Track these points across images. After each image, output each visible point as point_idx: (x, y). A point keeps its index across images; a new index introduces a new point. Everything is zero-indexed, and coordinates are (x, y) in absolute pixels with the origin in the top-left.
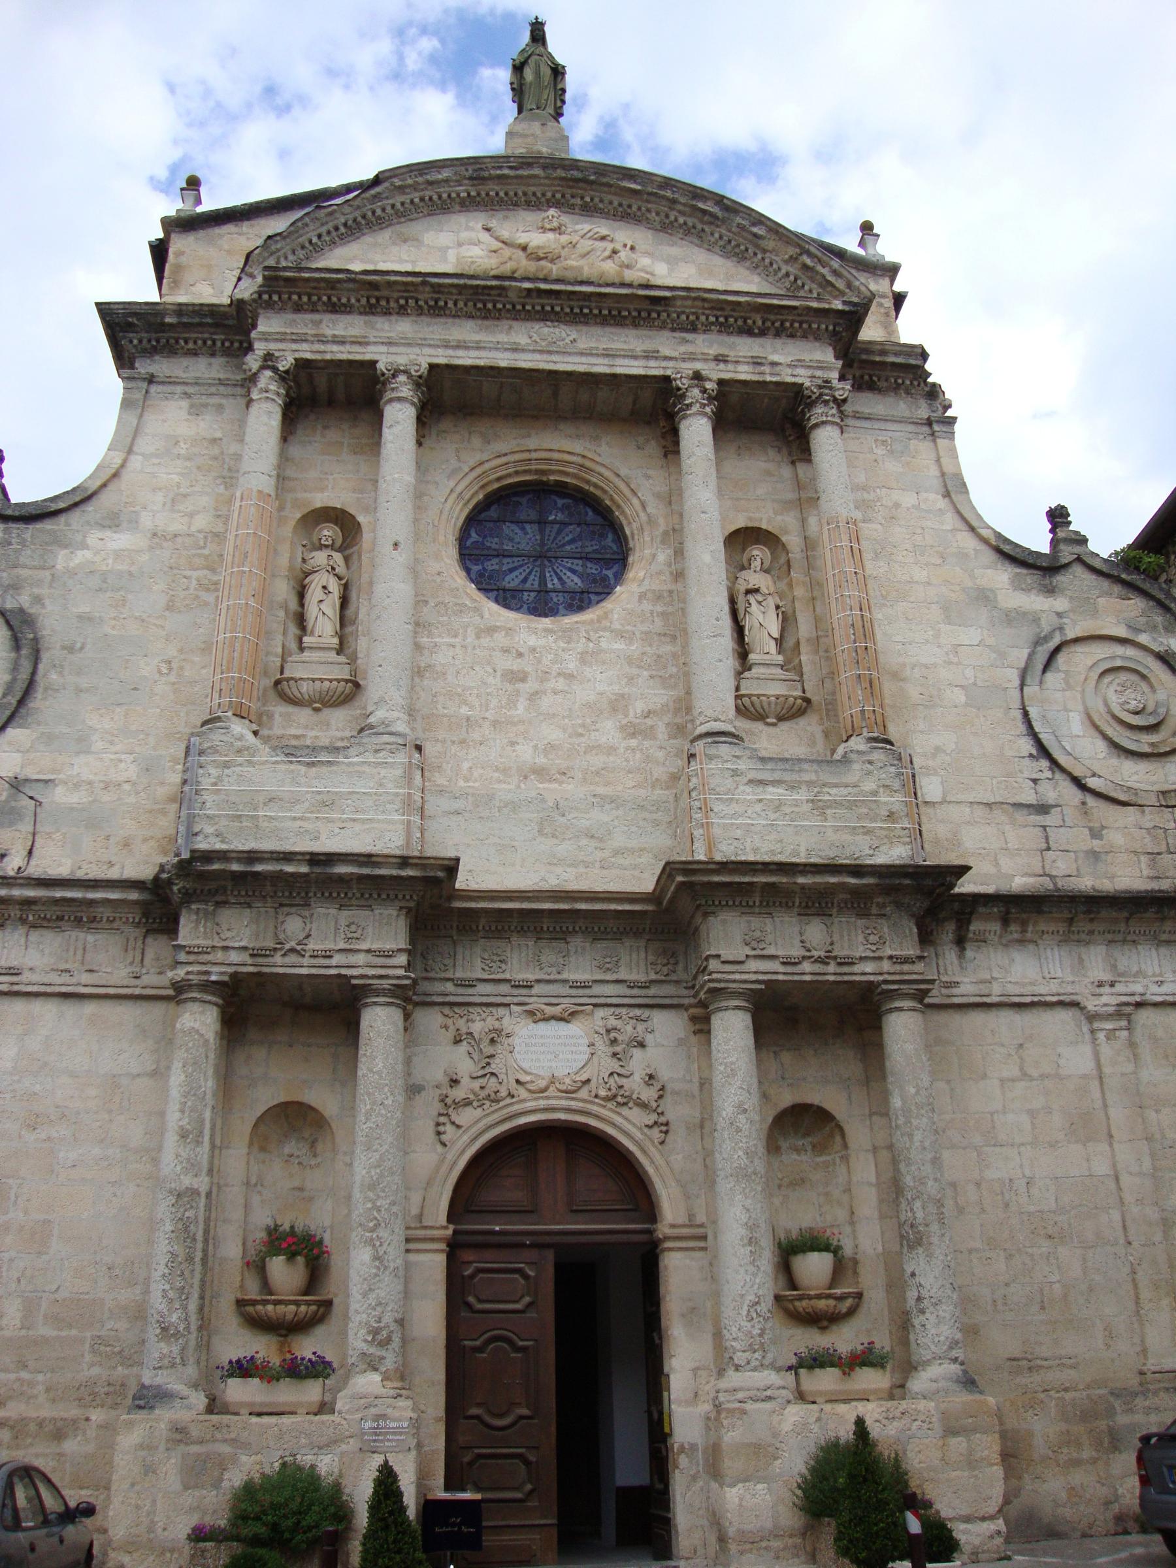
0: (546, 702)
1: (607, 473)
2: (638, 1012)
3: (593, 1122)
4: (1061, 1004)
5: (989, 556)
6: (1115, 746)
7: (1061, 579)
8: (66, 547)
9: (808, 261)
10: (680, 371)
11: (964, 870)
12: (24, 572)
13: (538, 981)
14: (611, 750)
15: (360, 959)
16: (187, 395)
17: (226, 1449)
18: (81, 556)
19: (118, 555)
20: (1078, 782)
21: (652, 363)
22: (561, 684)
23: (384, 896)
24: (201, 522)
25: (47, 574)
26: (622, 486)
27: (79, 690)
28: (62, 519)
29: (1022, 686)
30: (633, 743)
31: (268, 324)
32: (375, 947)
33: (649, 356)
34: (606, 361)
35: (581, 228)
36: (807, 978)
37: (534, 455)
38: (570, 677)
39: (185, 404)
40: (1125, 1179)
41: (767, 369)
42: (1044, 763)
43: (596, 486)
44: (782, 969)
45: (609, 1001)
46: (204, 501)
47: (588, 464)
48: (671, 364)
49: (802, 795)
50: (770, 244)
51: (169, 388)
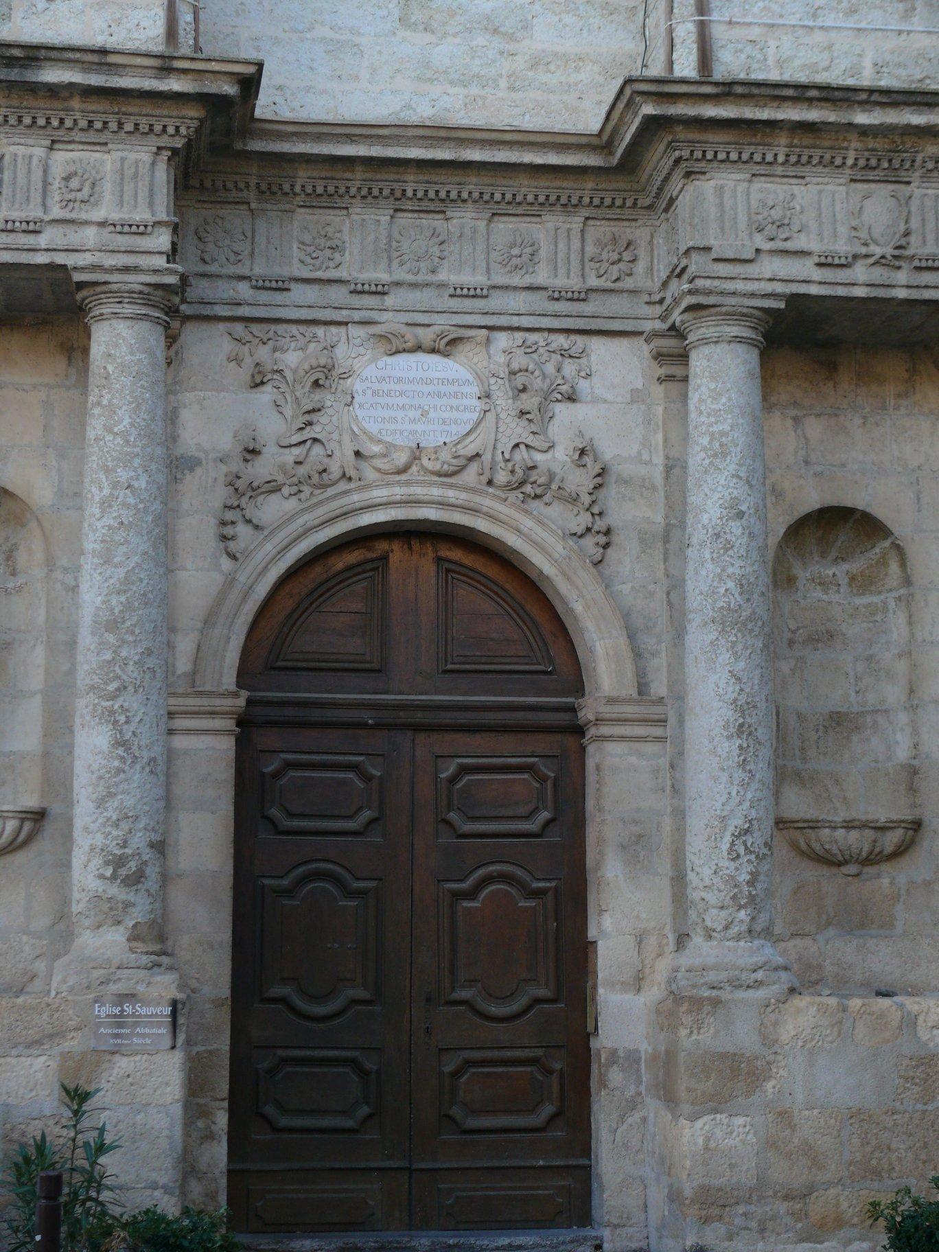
2: (561, 341)
13: (398, 284)
23: (129, 127)
32: (561, 282)
36: (860, 292)
44: (817, 274)
45: (515, 321)
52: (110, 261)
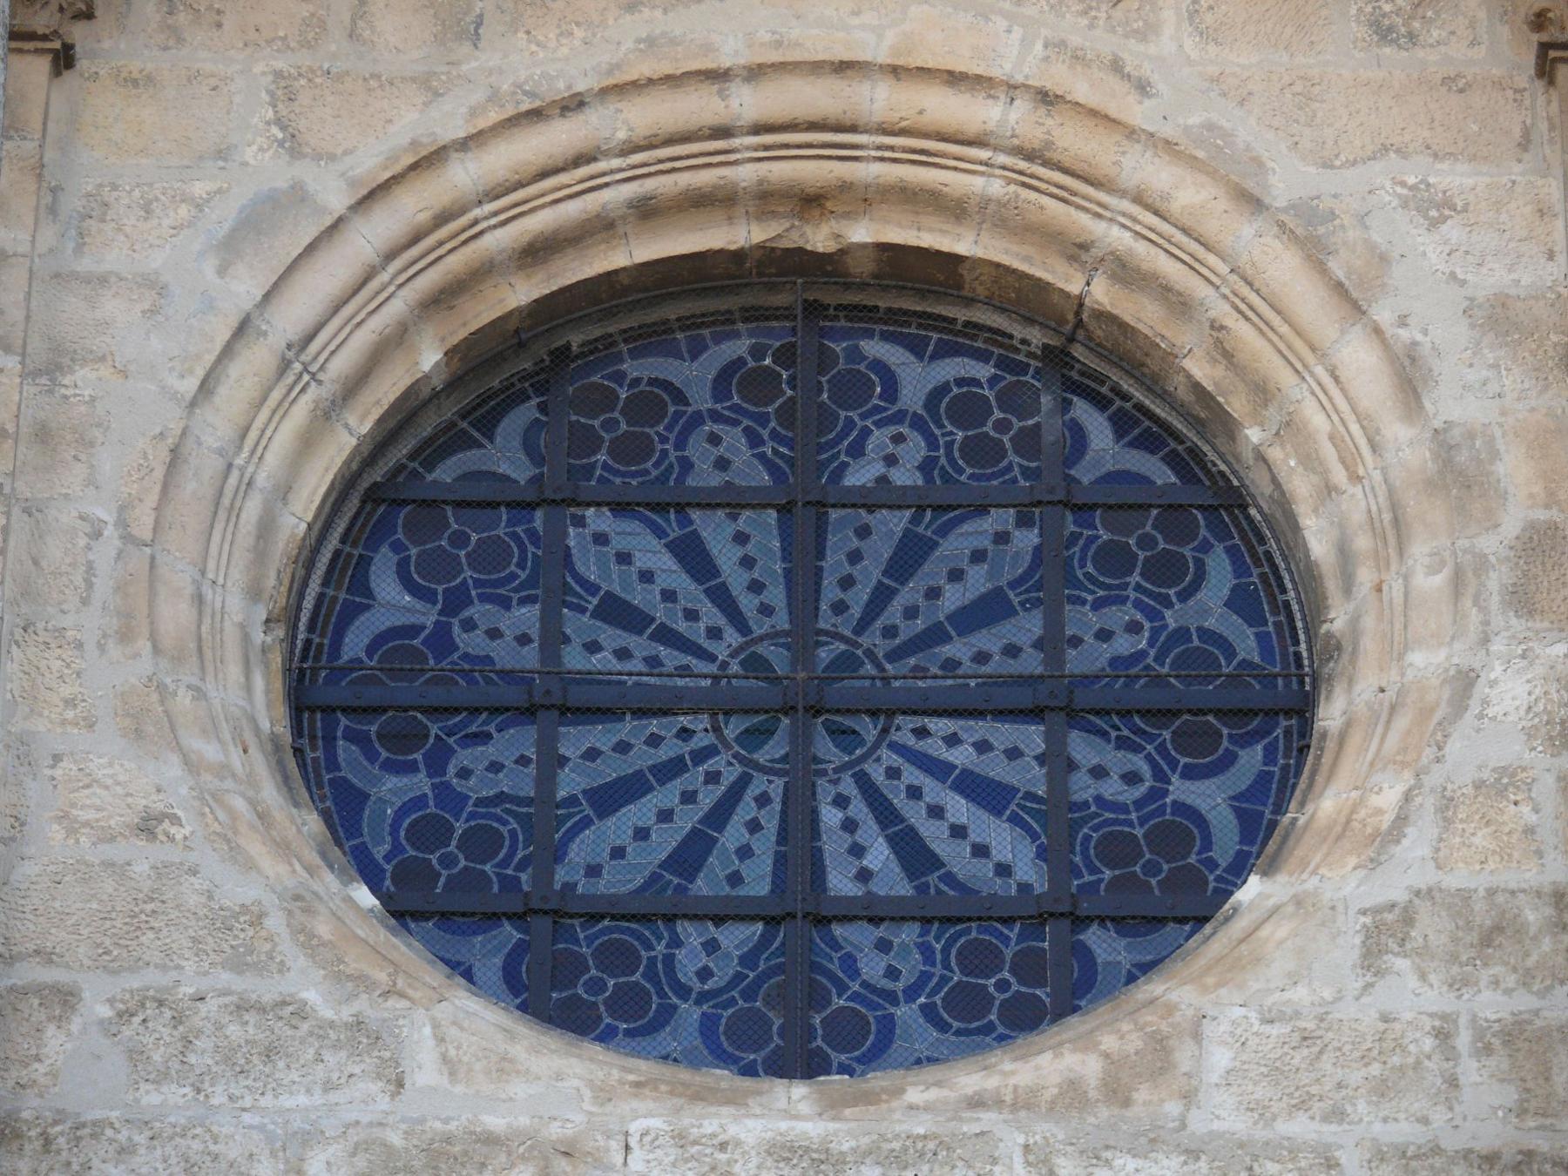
1: (1189, 194)
26: (1282, 268)
37: (747, 103)
47: (1073, 139)
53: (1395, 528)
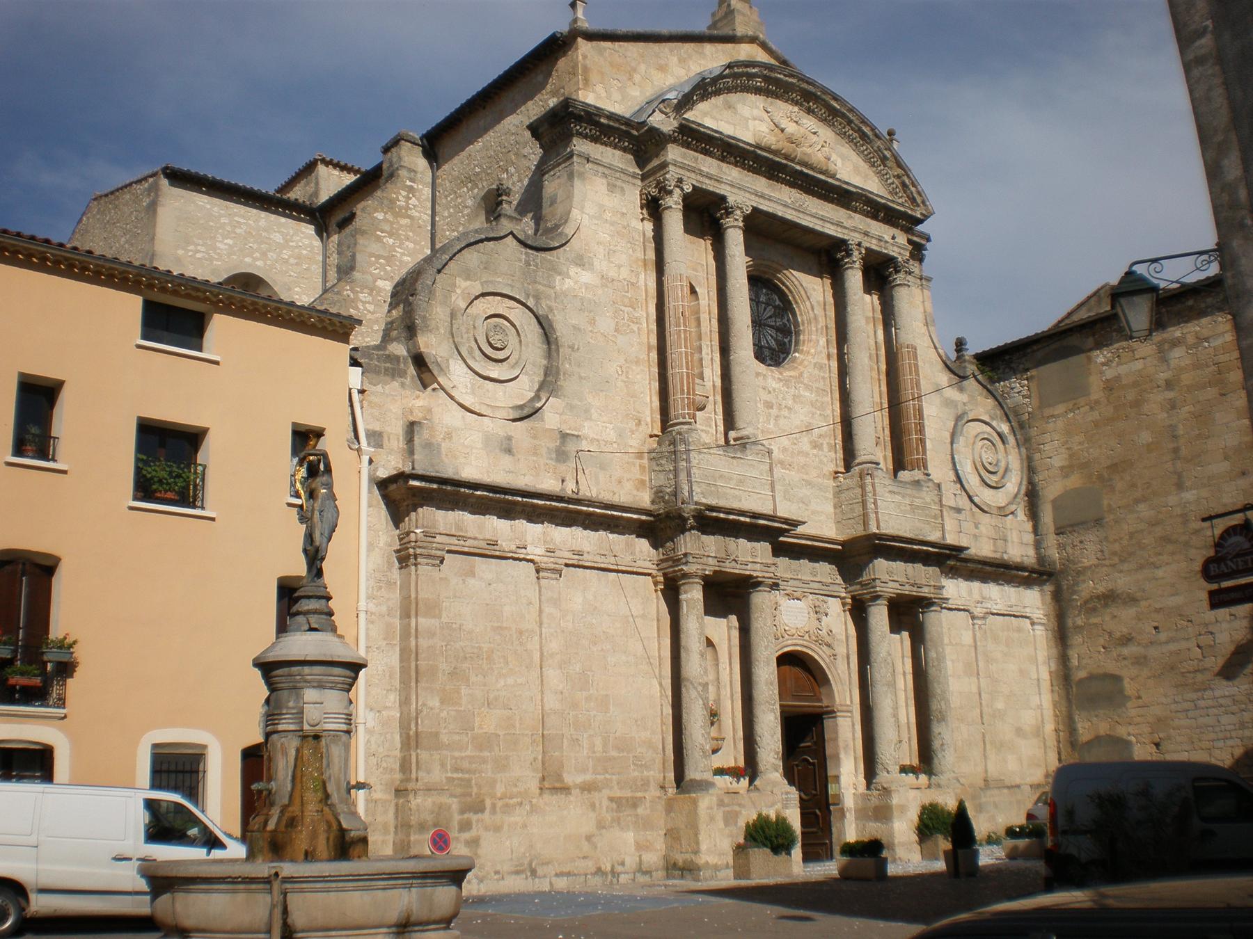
0: (782, 421)
3: (816, 657)
4: (964, 610)
5: (940, 365)
6: (983, 480)
7: (965, 383)
8: (560, 274)
9: (907, 181)
10: (853, 238)
11: (967, 548)
12: (540, 287)
14: (807, 455)
15: (758, 567)
16: (605, 176)
17: (737, 808)
18: (568, 283)
19: (587, 286)
20: (970, 498)
21: (839, 229)
22: (785, 412)
24: (625, 273)
25: (552, 292)
26: (803, 293)
27: (581, 378)
28: (555, 252)
29: (952, 443)
30: (815, 451)
31: (674, 153)
33: (839, 224)
34: (820, 223)
35: (809, 123)
38: (790, 409)
39: (604, 181)
40: (983, 696)
41: (874, 241)
42: (958, 486)
43: (787, 287)
46: (623, 259)
48: (845, 231)
49: (907, 501)
50: (891, 163)
51: (595, 167)
52: (767, 575)
53: (810, 322)
